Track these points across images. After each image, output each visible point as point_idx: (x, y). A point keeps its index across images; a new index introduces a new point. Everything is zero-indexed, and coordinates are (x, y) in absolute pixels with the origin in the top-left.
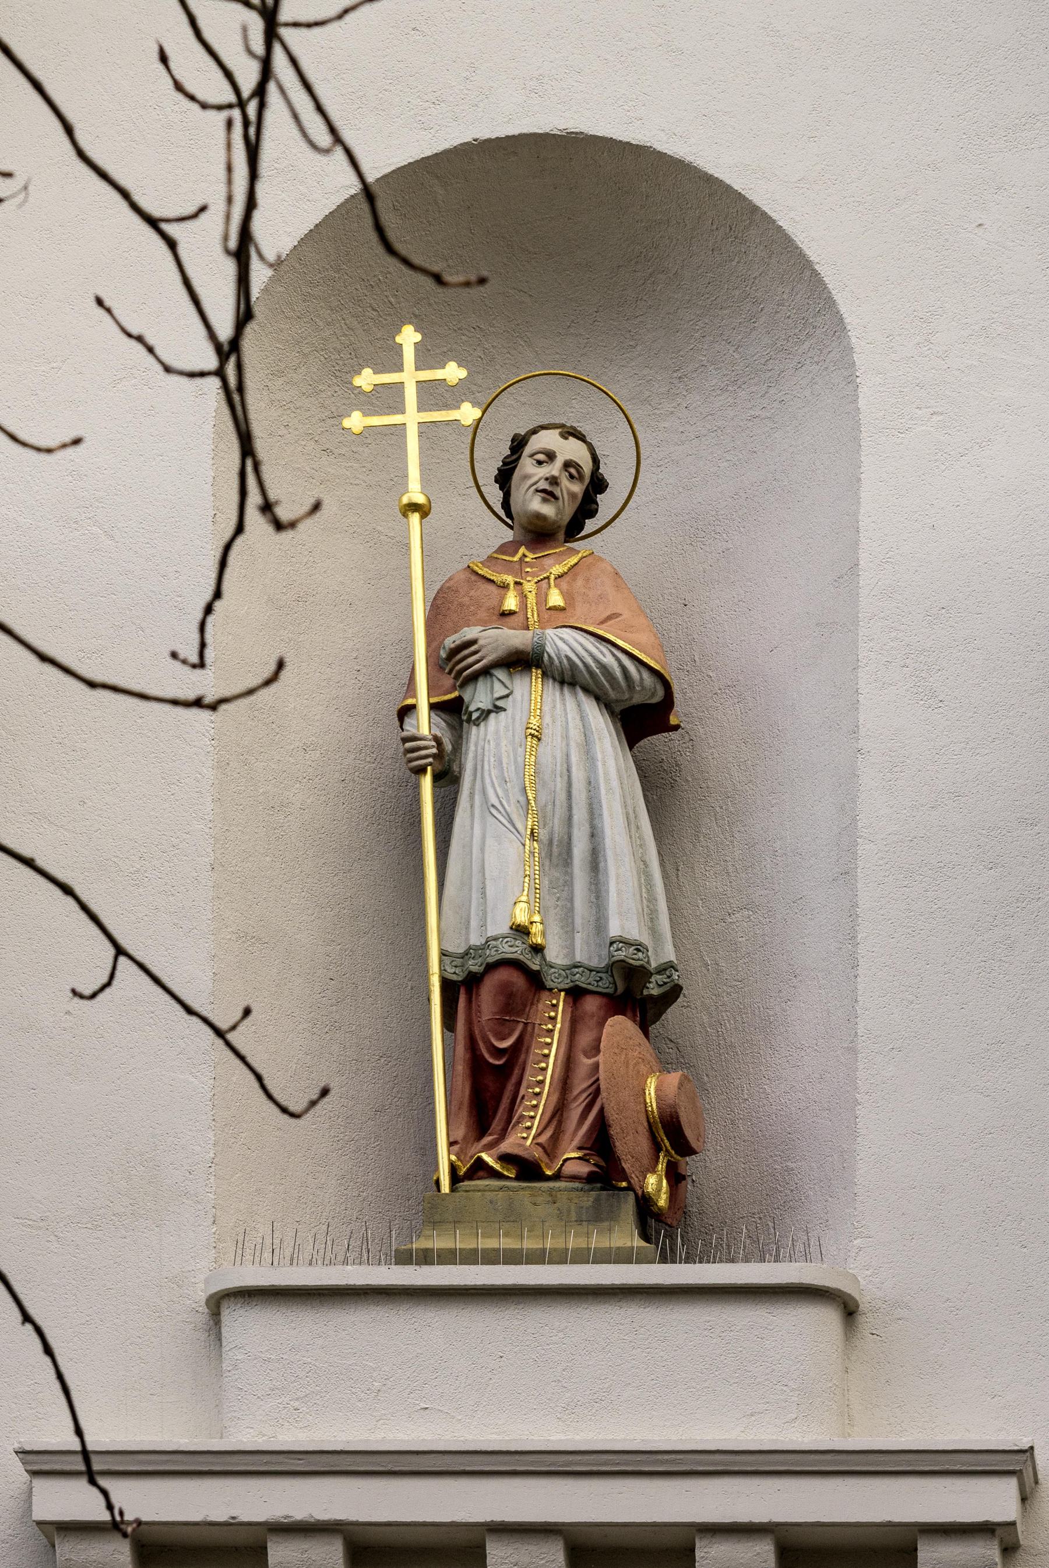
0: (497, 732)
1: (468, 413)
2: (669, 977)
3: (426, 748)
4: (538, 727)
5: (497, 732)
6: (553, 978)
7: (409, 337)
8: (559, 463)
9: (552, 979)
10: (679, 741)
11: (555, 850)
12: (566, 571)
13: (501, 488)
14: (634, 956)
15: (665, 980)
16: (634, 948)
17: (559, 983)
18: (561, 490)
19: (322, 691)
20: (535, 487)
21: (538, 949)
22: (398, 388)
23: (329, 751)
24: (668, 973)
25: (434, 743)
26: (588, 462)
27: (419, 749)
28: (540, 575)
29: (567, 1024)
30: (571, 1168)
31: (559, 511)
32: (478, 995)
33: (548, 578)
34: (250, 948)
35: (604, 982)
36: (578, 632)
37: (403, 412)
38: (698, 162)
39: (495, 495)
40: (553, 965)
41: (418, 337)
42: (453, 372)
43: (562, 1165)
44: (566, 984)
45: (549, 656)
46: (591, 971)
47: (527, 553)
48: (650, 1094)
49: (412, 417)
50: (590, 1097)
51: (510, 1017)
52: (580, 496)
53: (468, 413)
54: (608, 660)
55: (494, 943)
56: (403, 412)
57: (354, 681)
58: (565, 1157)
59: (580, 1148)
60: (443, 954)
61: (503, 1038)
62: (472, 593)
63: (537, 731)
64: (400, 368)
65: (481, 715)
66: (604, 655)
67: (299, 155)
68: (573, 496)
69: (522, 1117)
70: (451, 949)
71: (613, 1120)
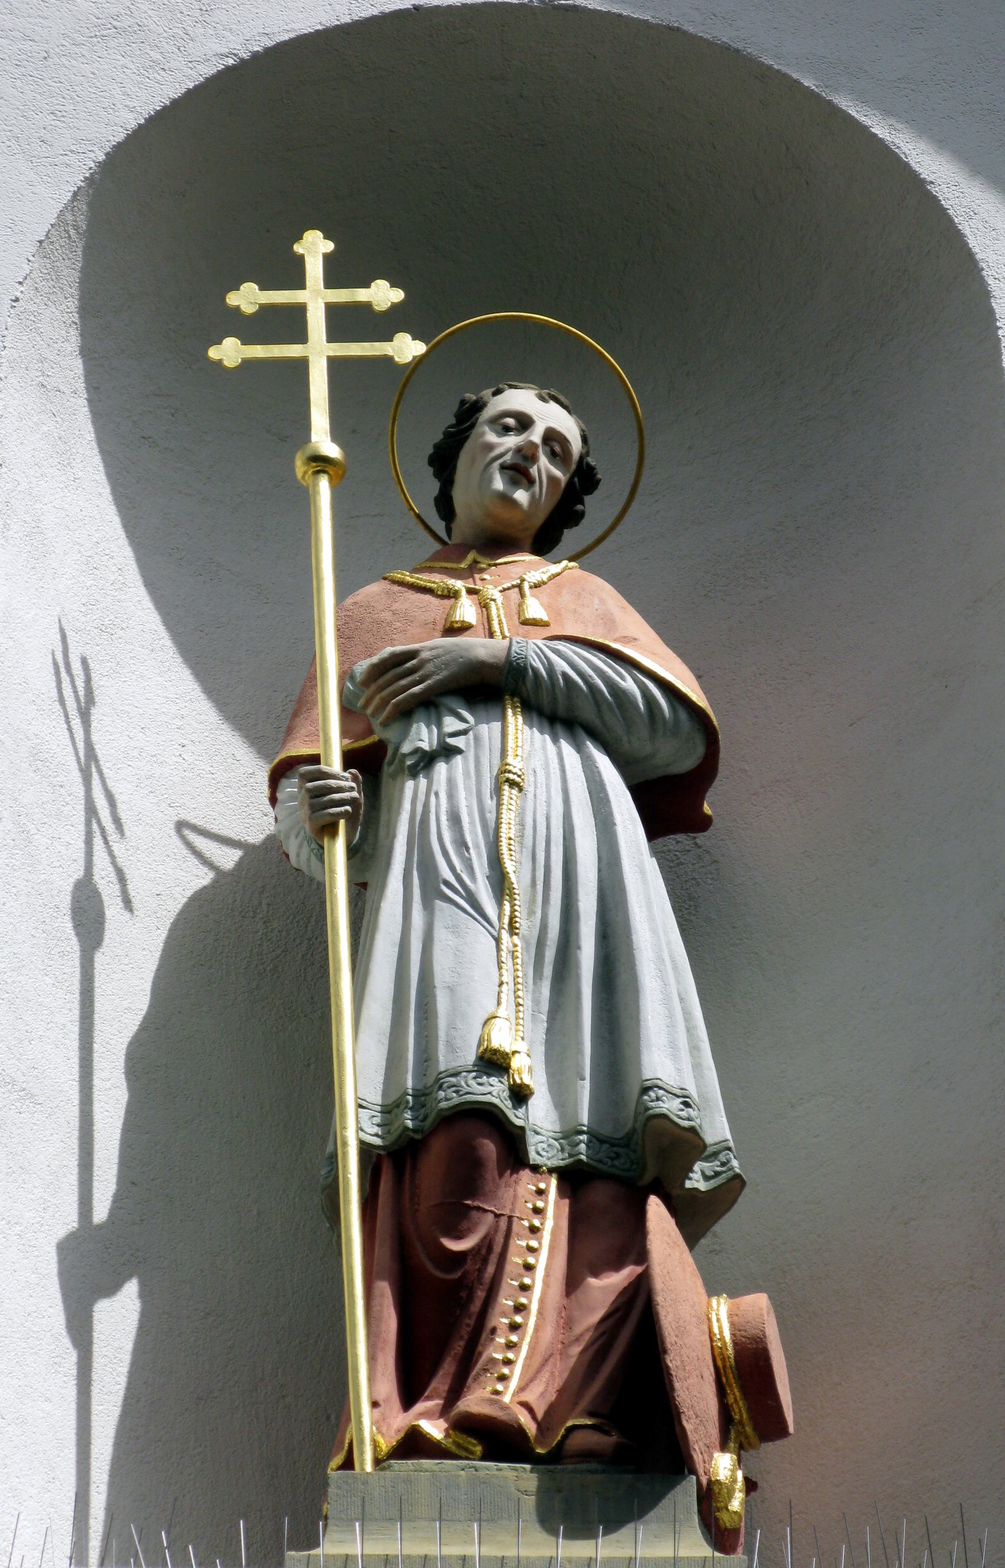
0: (451, 783)
2: (723, 1164)
4: (520, 770)
6: (540, 1149)
8: (536, 435)
10: (693, 864)
12: (545, 579)
13: (437, 475)
14: (680, 1113)
15: (719, 1169)
17: (549, 1159)
19: (130, 763)
20: (500, 461)
22: (299, 311)
23: (138, 849)
24: (722, 1157)
26: (578, 440)
28: (503, 584)
29: (564, 1224)
30: (580, 1441)
31: (534, 501)
34: (18, 1104)
35: (622, 1160)
36: (362, 940)
38: (749, 50)
40: (539, 1130)
41: (329, 246)
43: (565, 1437)
47: (479, 559)
48: (718, 1320)
50: (604, 1338)
52: (563, 484)
54: (628, 683)
55: (453, 1080)
57: (176, 759)
58: (570, 1423)
59: (591, 1414)
62: (395, 606)
63: (519, 776)
64: (299, 283)
67: (150, 12)
68: (552, 479)
69: (493, 1361)
71: (672, 1345)
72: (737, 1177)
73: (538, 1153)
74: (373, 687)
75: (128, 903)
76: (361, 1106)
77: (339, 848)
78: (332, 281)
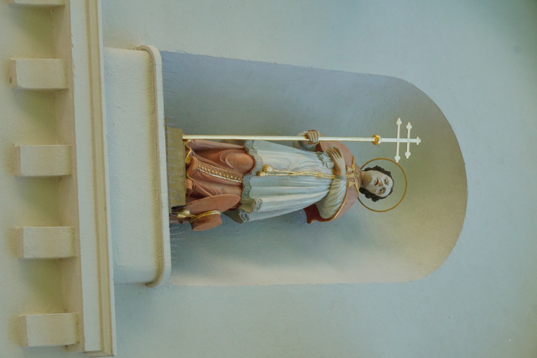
1: (397, 158)
3: (315, 139)
5: (317, 162)
7: (418, 141)
9: (246, 178)
11: (285, 181)
13: (374, 168)
16: (258, 207)
18: (377, 187)
21: (258, 174)
24: (246, 219)
25: (316, 141)
27: (315, 137)
32: (241, 152)
33: (355, 182)
37: (400, 138)
39: (372, 165)
41: (418, 144)
42: (408, 154)
44: (244, 183)
45: (339, 181)
46: (249, 192)
49: (398, 140)
51: (188, 158)
53: (397, 158)
56: (400, 138)
59: (195, 186)
60: (253, 141)
61: (228, 161)
64: (411, 138)
65: (321, 158)
66: (340, 199)
68: (375, 190)
70: (254, 144)
72: (242, 222)
73: (245, 178)
74: (334, 149)
75: (358, 178)
76: (253, 141)
77: (303, 139)
78: (411, 144)
